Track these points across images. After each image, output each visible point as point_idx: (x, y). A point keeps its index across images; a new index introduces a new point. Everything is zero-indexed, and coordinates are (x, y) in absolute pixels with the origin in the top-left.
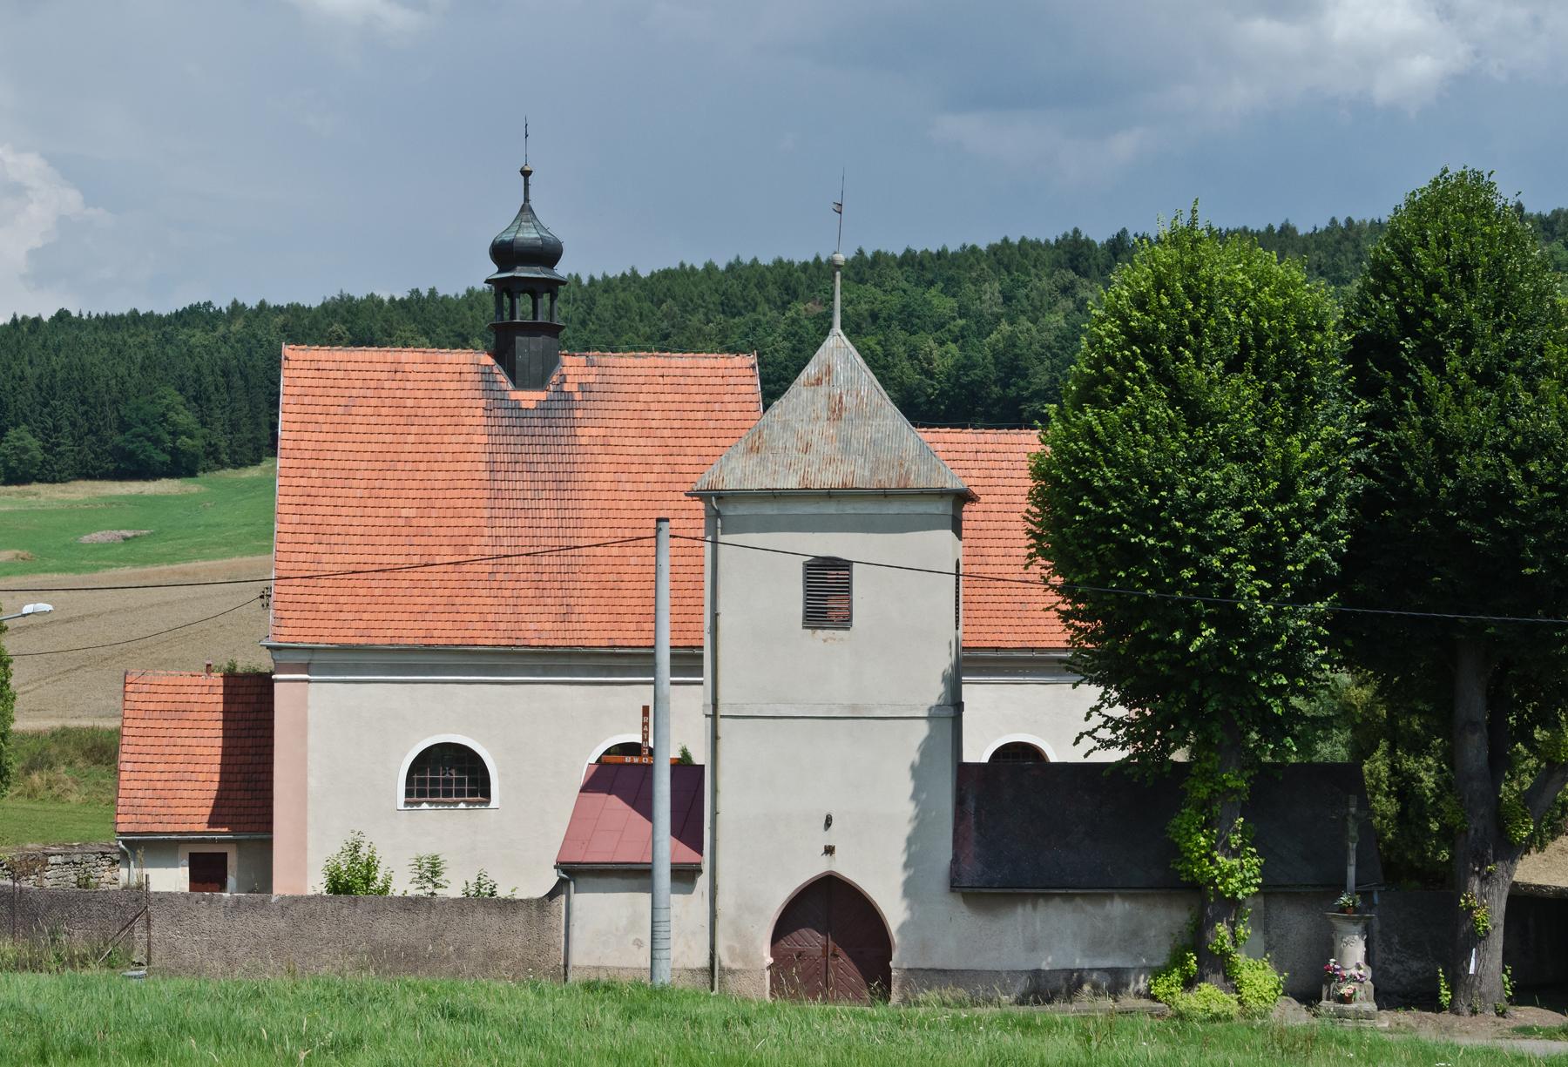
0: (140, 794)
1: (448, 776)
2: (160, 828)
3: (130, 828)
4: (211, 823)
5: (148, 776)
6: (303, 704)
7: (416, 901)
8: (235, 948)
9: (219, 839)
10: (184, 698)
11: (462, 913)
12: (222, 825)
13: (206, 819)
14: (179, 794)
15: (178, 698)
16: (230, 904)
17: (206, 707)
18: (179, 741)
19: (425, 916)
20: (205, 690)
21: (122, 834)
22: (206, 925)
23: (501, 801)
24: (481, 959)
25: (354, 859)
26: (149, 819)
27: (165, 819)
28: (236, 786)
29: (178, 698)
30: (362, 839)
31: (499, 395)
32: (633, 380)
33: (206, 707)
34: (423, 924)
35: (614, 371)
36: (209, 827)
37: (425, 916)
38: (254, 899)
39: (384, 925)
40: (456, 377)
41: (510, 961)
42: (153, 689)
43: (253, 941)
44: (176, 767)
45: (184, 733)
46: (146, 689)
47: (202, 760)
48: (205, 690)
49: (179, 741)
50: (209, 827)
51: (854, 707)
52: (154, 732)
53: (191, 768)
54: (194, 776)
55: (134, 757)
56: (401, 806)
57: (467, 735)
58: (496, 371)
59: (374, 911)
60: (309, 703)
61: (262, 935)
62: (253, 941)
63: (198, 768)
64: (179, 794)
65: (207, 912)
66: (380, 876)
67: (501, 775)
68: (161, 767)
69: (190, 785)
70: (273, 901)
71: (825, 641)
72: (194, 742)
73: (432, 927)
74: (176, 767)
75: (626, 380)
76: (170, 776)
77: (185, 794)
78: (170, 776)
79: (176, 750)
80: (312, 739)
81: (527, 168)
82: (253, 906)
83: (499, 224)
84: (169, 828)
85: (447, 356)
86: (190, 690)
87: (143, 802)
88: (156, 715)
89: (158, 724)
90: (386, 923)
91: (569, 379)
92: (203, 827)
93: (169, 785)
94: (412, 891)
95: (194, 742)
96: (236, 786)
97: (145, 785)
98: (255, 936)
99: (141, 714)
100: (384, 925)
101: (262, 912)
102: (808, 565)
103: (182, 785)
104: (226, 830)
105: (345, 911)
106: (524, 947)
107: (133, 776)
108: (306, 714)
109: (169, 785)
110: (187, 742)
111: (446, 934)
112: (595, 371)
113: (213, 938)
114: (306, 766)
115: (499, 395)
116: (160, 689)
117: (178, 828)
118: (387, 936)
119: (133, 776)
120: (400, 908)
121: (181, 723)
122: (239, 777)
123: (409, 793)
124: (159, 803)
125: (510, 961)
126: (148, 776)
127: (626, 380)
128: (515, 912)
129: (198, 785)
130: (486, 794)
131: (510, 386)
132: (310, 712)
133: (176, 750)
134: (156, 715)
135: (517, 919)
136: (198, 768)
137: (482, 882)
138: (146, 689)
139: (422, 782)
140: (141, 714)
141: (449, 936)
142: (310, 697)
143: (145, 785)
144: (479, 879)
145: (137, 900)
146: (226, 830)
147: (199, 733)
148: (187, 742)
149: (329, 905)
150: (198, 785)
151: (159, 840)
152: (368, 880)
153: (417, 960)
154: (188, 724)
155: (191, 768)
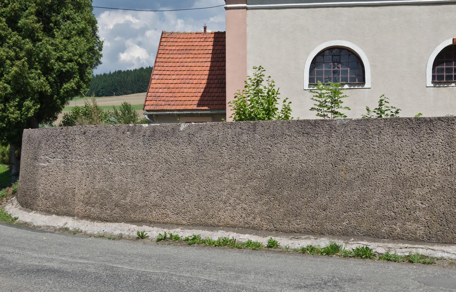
0: (161, 90)
1: (336, 68)
2: (168, 108)
3: (152, 108)
4: (199, 105)
5: (166, 81)
6: (244, 22)
7: (314, 124)
8: (151, 172)
9: (200, 114)
10: (191, 44)
11: (366, 135)
12: (204, 105)
13: (196, 102)
14: (182, 90)
15: (188, 44)
16: (148, 133)
17: (202, 48)
18: (186, 64)
19: (325, 139)
20: (203, 40)
21: (147, 111)
22: (130, 152)
23: (372, 83)
24: (390, 187)
25: (258, 93)
26: (163, 103)
27: (172, 103)
28: (213, 86)
29: (188, 44)
30: (263, 73)
33: (202, 48)
34: (322, 149)
36: (198, 107)
37: (325, 139)
38: (166, 127)
39: (283, 150)
41: (426, 190)
42: (176, 40)
43: (165, 166)
44: (182, 77)
45: (189, 60)
46: (172, 40)
47: (196, 73)
48: (203, 40)
49: (186, 64)
50: (198, 107)
52: (173, 60)
53: (190, 77)
54: (191, 81)
55: (160, 73)
56: (306, 87)
57: (349, 41)
59: (273, 136)
60: (248, 22)
61: (172, 160)
62: (165, 166)
63: (194, 77)
64: (182, 90)
65: (131, 141)
66: (279, 105)
67: (373, 66)
68: (174, 77)
69: (189, 86)
70: (181, 129)
72: (194, 64)
73: (333, 151)
74: (182, 77)
76: (179, 81)
77: (185, 90)
78: (179, 81)
79: (184, 68)
80: (249, 46)
82: (165, 135)
84: (174, 108)
86: (194, 40)
87: (162, 95)
88: (175, 52)
89: (176, 56)
90: (285, 148)
92: (195, 107)
93: (177, 86)
94: (313, 116)
95: (194, 64)
96: (213, 86)
97: (164, 86)
98: (167, 161)
99: (167, 52)
100: (283, 150)
101: (173, 139)
103: (184, 86)
104: (206, 108)
105: (245, 137)
106: (445, 174)
107: (159, 81)
108: (245, 29)
109: (177, 86)
110: (190, 64)
111: (348, 157)
113: (135, 164)
114: (246, 62)
116: (179, 40)
117: (178, 108)
118: (285, 161)
119: (159, 81)
120: (298, 132)
121: (188, 56)
122: (216, 81)
123: (311, 80)
124: (170, 95)
125: (426, 190)
126: (166, 81)
128: (431, 132)
129: (193, 86)
130: (363, 81)
132: (248, 29)
133: (184, 68)
134: (175, 52)
135: (434, 140)
136: (194, 77)
137: (384, 108)
138: (172, 40)
139: (320, 73)
140: (167, 52)
141: (352, 161)
142: (248, 19)
143: (164, 86)
144: (380, 105)
145: (85, 133)
146: (206, 108)
147: (197, 60)
148: (190, 64)
149: (230, 131)
150: (193, 86)
151: (167, 114)
152: (269, 112)
153: (317, 186)
154: (191, 56)
155: (190, 77)
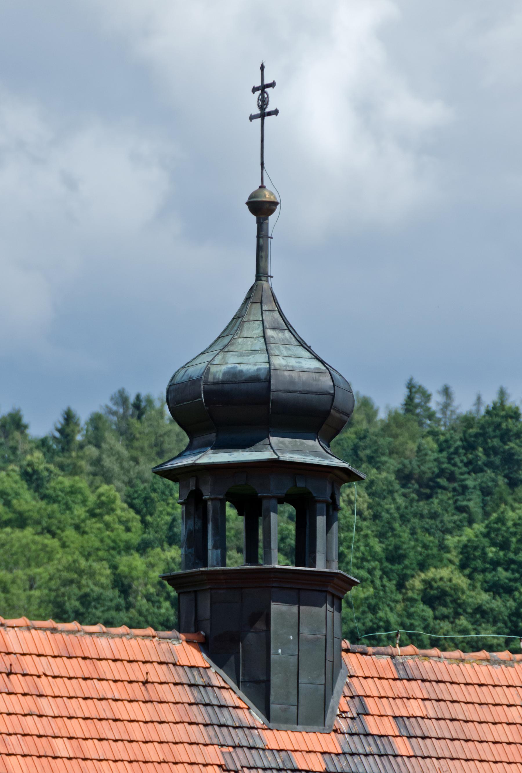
31: (239, 737)
32: (499, 714)
35: (456, 692)
40: (137, 691)
58: (216, 681)
75: (485, 714)
81: (267, 196)
85: (102, 642)
91: (371, 705)
112: (415, 688)
115: (239, 737)
127: (485, 714)
131: (258, 720)
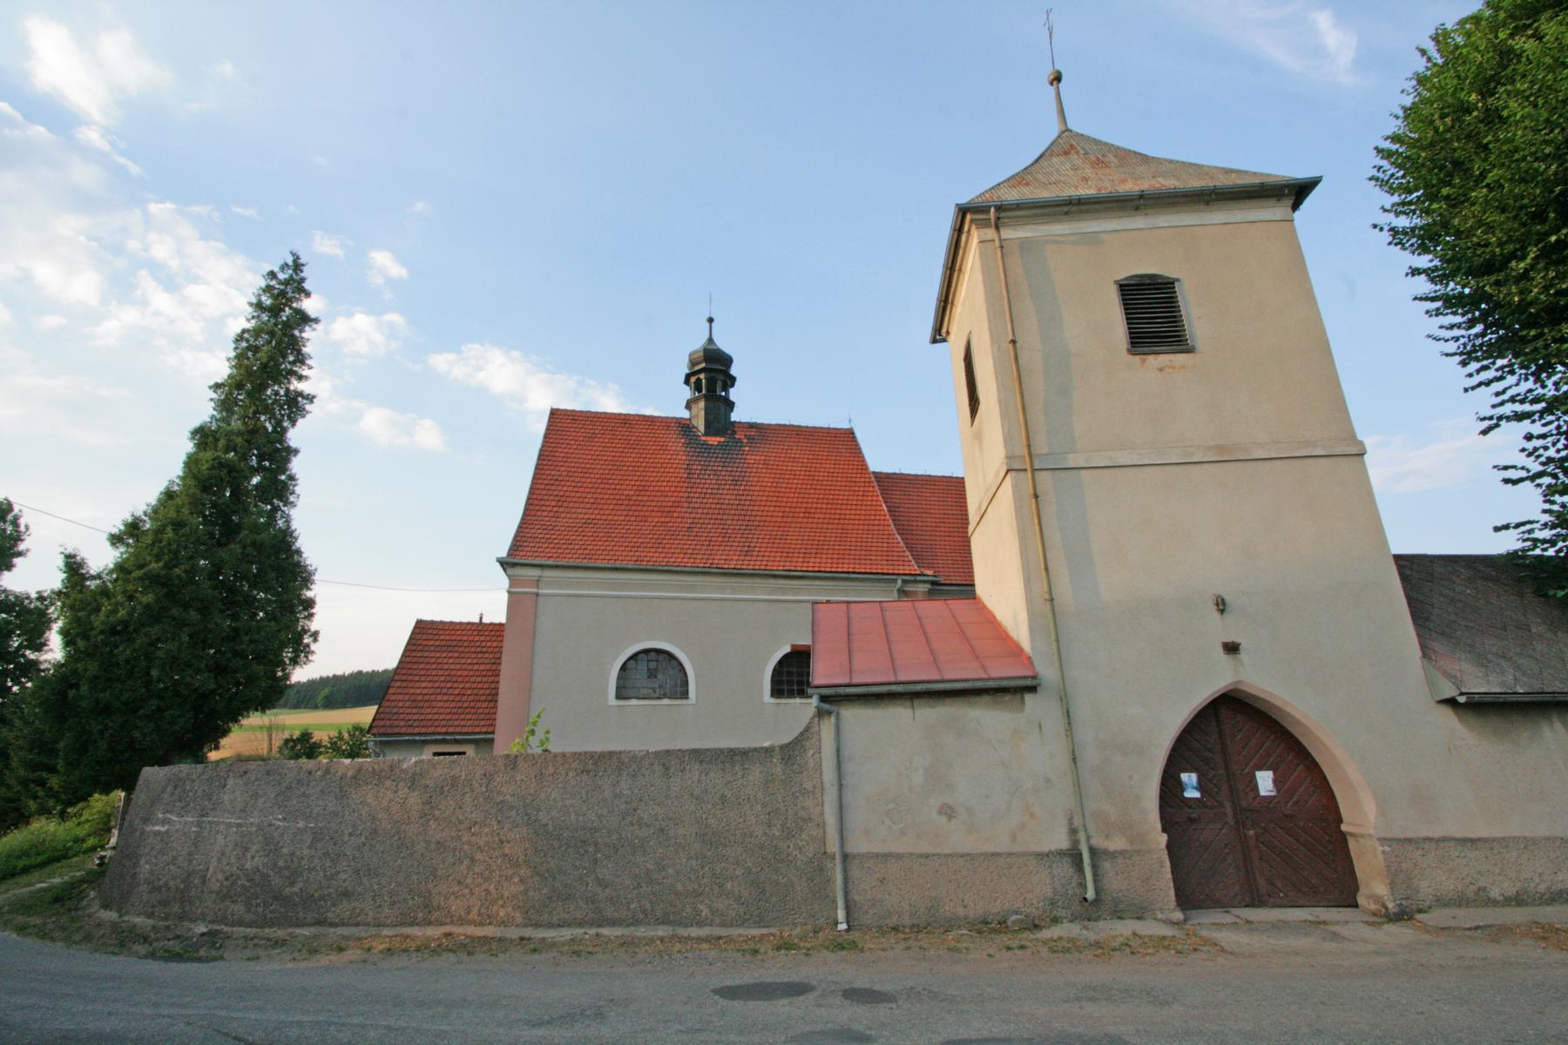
51: (1220, 448)
71: (1161, 370)
83: (698, 343)
102: (1121, 286)
